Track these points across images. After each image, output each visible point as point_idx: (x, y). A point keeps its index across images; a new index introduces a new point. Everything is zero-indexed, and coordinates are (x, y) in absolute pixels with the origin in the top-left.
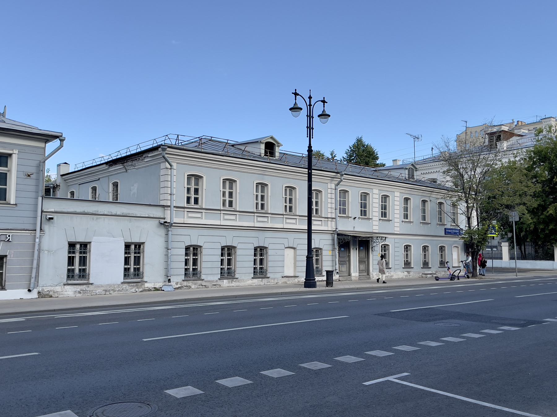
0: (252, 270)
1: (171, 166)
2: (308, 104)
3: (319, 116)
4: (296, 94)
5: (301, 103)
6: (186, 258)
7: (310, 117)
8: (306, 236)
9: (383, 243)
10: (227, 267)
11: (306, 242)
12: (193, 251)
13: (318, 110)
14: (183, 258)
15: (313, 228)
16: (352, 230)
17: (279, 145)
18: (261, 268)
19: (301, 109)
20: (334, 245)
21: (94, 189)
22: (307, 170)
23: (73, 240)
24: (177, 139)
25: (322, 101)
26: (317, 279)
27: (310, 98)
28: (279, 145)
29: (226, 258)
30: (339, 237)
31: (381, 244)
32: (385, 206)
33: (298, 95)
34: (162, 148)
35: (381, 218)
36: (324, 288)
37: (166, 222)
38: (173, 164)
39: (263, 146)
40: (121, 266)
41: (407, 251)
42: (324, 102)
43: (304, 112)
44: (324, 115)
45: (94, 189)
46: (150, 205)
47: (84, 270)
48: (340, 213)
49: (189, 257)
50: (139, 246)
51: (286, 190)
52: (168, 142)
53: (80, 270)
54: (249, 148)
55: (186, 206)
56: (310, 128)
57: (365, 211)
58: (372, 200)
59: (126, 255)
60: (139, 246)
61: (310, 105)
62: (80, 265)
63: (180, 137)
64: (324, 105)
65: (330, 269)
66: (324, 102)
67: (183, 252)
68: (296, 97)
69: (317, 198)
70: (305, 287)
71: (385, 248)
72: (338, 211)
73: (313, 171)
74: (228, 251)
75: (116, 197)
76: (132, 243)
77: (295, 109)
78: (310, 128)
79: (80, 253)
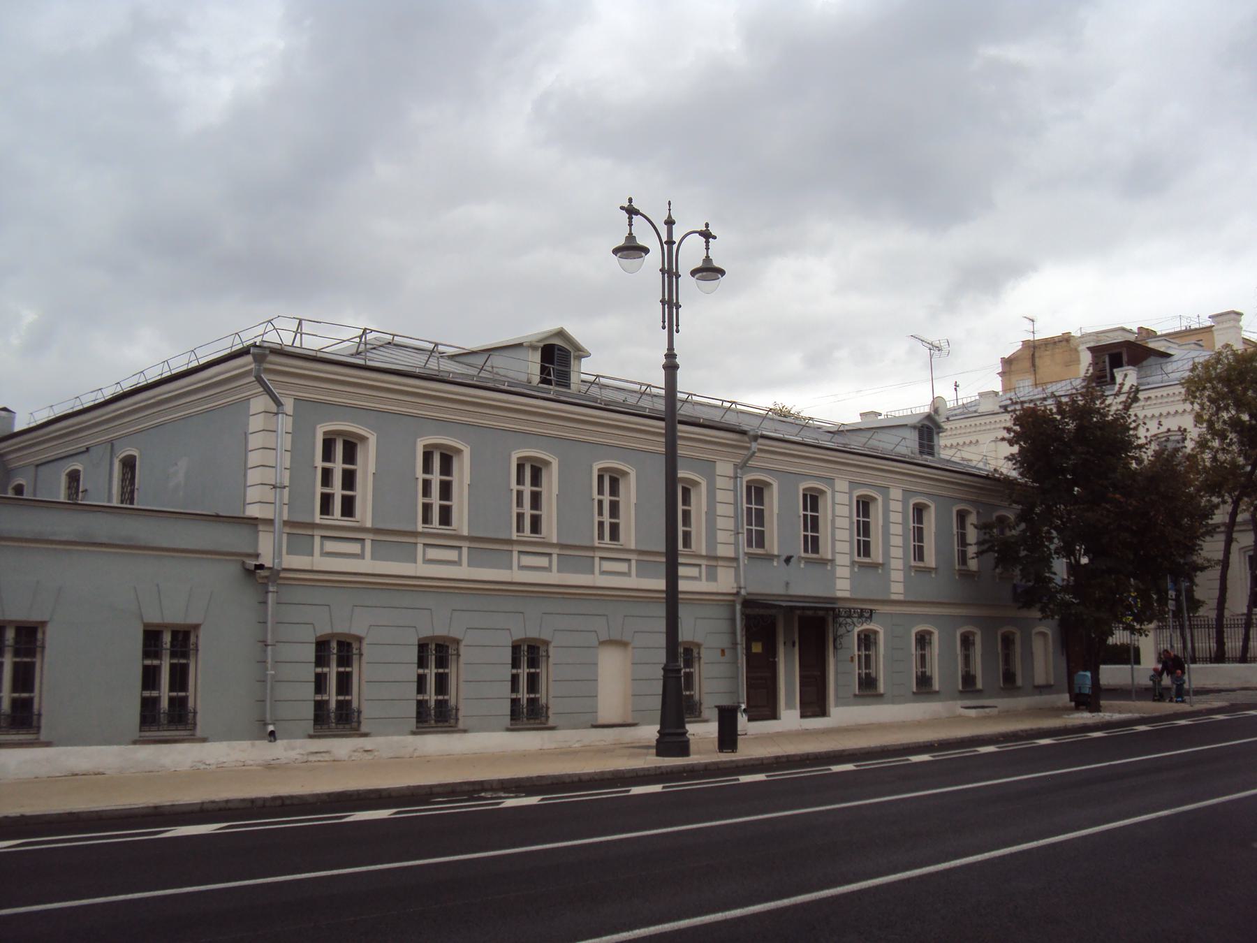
0: (412, 710)
1: (278, 403)
2: (664, 239)
3: (694, 273)
4: (631, 211)
5: (645, 237)
6: (319, 670)
7: (670, 273)
8: (661, 611)
9: (865, 626)
10: (526, 696)
11: (662, 625)
12: (337, 651)
13: (691, 254)
14: (310, 672)
15: (683, 585)
16: (781, 591)
17: (581, 353)
18: (439, 703)
19: (646, 250)
20: (734, 633)
21: (74, 477)
22: (662, 424)
23: (154, 618)
24: (299, 331)
25: (701, 233)
26: (692, 729)
27: (670, 223)
28: (581, 353)
29: (431, 672)
30: (749, 611)
31: (857, 630)
32: (815, 520)
33: (637, 213)
34: (254, 356)
35: (856, 558)
36: (652, 761)
37: (261, 567)
38: (283, 400)
39: (537, 357)
40: (133, 694)
41: (923, 648)
42: (707, 235)
43: (654, 259)
44: (708, 271)
45: (74, 477)
46: (217, 517)
47: (28, 703)
48: (750, 544)
49: (326, 670)
50: (183, 639)
51: (601, 478)
52: (272, 338)
53: (171, 700)
54: (497, 361)
55: (597, 544)
56: (670, 304)
57: (815, 540)
58: (833, 510)
59: (148, 662)
60: (183, 639)
61: (670, 242)
62: (172, 689)
63: (306, 327)
64: (707, 243)
65: (725, 701)
66: (707, 235)
67: (310, 653)
68: (630, 219)
69: (686, 501)
70: (659, 754)
71: (867, 640)
72: (743, 538)
73: (680, 427)
74: (437, 653)
75: (128, 492)
76: (166, 626)
77: (631, 249)
78: (670, 304)
79: (173, 655)
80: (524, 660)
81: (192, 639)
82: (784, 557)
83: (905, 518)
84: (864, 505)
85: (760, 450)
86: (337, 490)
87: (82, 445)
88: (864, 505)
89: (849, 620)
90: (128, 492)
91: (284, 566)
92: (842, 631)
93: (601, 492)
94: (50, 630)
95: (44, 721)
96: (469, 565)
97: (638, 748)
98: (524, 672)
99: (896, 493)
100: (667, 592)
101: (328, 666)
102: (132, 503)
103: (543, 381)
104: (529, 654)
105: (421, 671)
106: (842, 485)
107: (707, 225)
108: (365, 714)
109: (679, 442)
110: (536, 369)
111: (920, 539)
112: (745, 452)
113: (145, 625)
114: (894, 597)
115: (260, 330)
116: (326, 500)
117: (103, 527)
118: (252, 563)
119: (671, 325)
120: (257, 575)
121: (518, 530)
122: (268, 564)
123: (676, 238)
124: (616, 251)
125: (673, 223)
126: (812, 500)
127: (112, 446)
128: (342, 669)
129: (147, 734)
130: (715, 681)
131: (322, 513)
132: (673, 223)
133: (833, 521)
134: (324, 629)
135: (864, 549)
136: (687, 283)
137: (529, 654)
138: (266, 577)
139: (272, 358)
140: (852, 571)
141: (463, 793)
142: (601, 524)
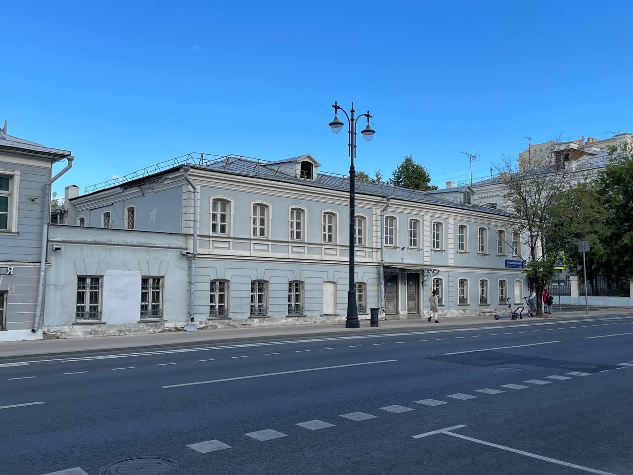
2: (350, 118)
3: (363, 132)
4: (336, 107)
5: (342, 118)
7: (352, 133)
8: (347, 269)
9: (435, 277)
10: (294, 303)
12: (220, 286)
14: (208, 294)
15: (356, 259)
19: (342, 124)
20: (379, 279)
22: (349, 194)
23: (83, 273)
25: (366, 115)
27: (352, 111)
30: (385, 270)
33: (339, 108)
34: (184, 169)
39: (299, 167)
42: (368, 116)
43: (346, 128)
45: (107, 215)
47: (96, 308)
49: (214, 293)
50: (157, 280)
53: (91, 307)
56: (352, 146)
59: (144, 291)
60: (157, 280)
61: (352, 120)
62: (91, 302)
65: (375, 306)
66: (368, 116)
70: (346, 327)
71: (437, 282)
72: (384, 240)
73: (356, 195)
74: (259, 286)
75: (131, 224)
76: (150, 277)
77: (336, 124)
78: (352, 146)
80: (294, 288)
81: (161, 281)
82: (401, 248)
83: (455, 231)
84: (438, 225)
85: (391, 204)
86: (258, 226)
87: (110, 202)
88: (438, 225)
89: (429, 274)
90: (131, 224)
91: (198, 253)
92: (426, 278)
93: (325, 222)
94: (166, 279)
95: (164, 312)
96: (233, 249)
97: (338, 325)
98: (293, 294)
99: (451, 221)
100: (350, 262)
101: (216, 292)
102: (133, 227)
103: (301, 177)
104: (296, 286)
105: (290, 293)
106: (427, 218)
107: (368, 112)
108: (305, 308)
109: (355, 201)
110: (299, 172)
111: (482, 242)
112: (385, 205)
113: (78, 276)
114: (450, 265)
115: (186, 158)
116: (214, 226)
117: (90, 236)
118: (184, 252)
119: (352, 155)
120: (189, 256)
121: (291, 238)
122: (192, 252)
123: (355, 118)
124: (330, 124)
125: (354, 111)
126: (414, 223)
127: (123, 202)
128: (221, 293)
129: (143, 319)
130: (372, 297)
131: (213, 231)
132: (354, 111)
133: (423, 233)
134: (214, 277)
135: (436, 244)
136: (359, 137)
137: (296, 286)
138: (191, 257)
139: (191, 170)
140: (431, 254)
141: (431, 328)
142: (325, 235)
